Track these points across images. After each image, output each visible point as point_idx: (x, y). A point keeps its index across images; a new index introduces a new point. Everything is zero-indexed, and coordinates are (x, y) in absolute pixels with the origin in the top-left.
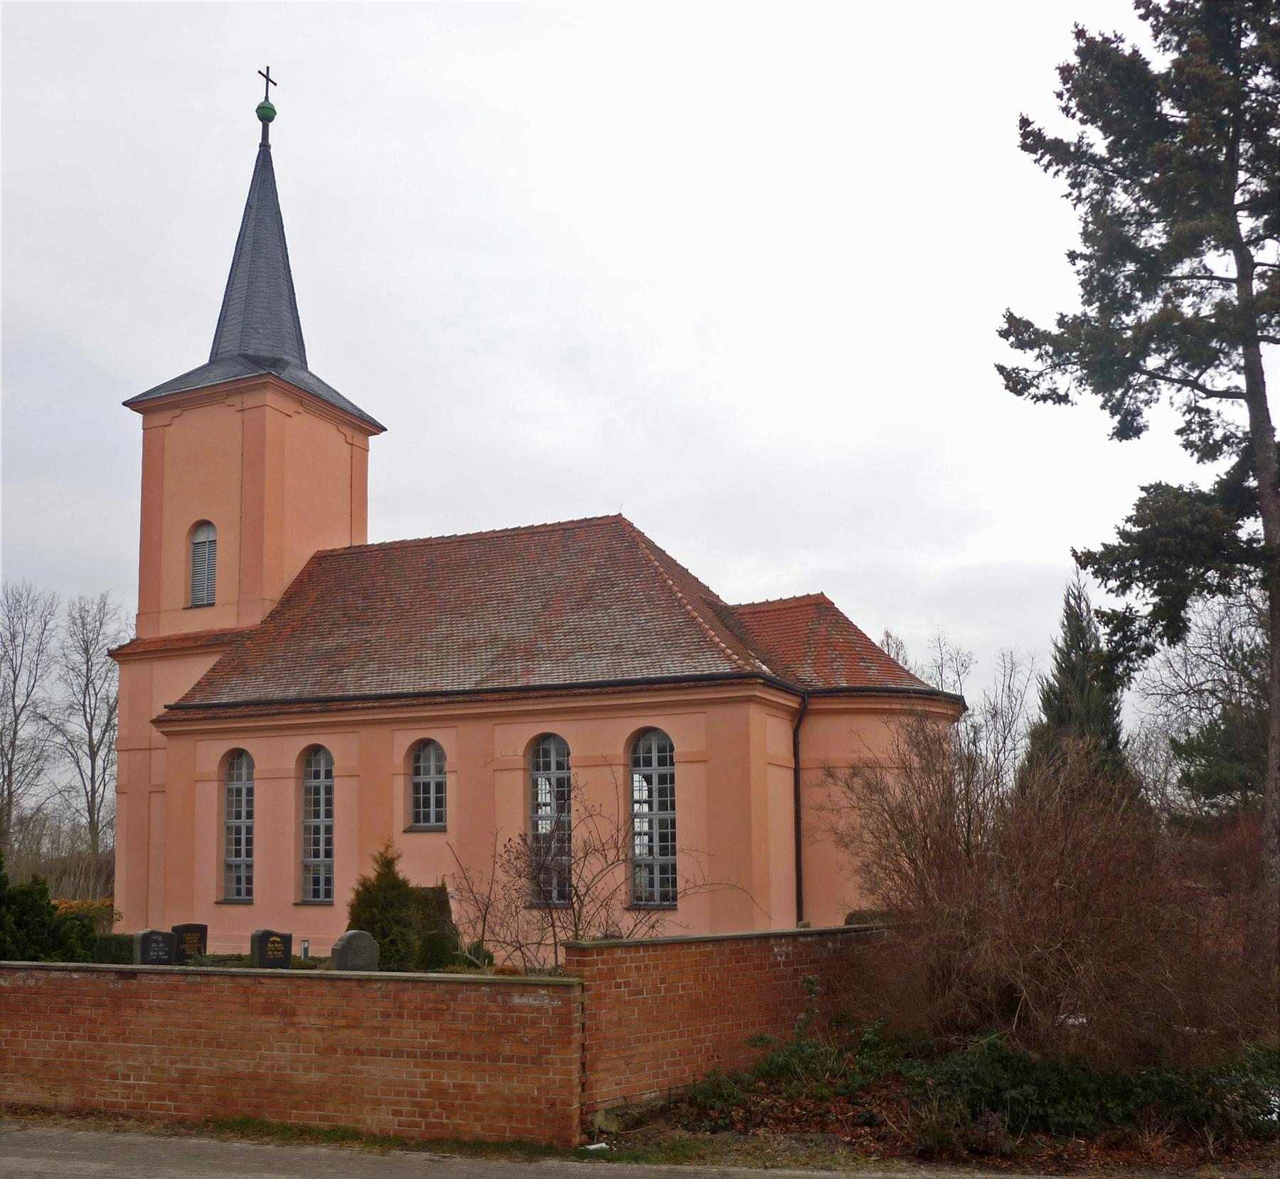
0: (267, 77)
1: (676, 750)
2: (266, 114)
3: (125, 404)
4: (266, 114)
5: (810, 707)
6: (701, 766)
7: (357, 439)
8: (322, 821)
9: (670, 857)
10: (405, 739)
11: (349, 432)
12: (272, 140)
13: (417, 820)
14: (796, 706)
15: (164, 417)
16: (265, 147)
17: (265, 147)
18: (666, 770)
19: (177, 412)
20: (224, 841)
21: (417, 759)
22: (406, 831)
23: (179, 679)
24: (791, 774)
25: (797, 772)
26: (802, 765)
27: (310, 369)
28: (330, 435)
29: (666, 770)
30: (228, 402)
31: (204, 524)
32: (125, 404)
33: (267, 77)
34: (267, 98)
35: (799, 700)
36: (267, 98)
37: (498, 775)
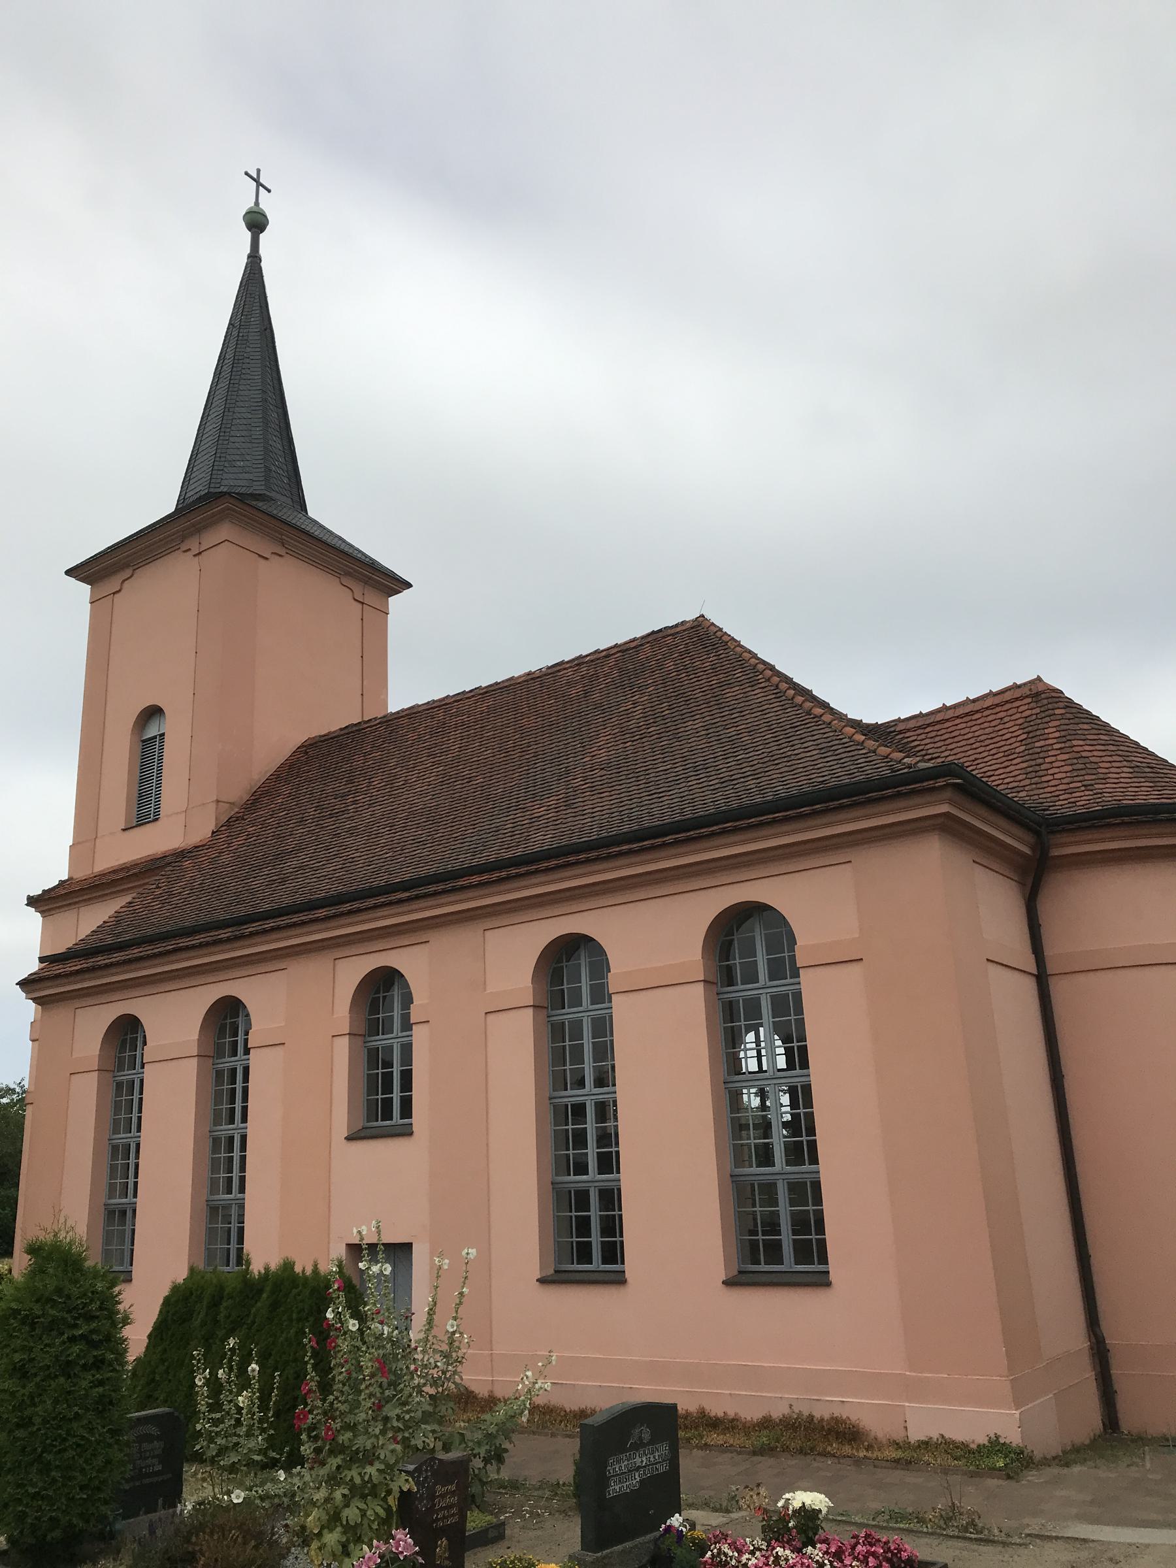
0: (259, 184)
1: (800, 942)
2: (256, 223)
3: (69, 572)
4: (256, 223)
5: (1055, 852)
6: (855, 968)
7: (371, 597)
8: (593, 1177)
9: (807, 1167)
10: (352, 971)
11: (358, 590)
12: (263, 251)
13: (371, 1115)
14: (1026, 850)
15: (113, 584)
16: (254, 260)
17: (254, 260)
18: (782, 987)
19: (128, 572)
20: (106, 1170)
21: (374, 1007)
22: (348, 1139)
23: (89, 921)
24: (1029, 986)
25: (1042, 979)
26: (1051, 968)
27: (310, 514)
28: (330, 595)
29: (782, 987)
30: (184, 547)
31: (153, 713)
32: (69, 572)
33: (259, 184)
34: (257, 203)
35: (1030, 838)
36: (257, 203)
37: (491, 1017)
